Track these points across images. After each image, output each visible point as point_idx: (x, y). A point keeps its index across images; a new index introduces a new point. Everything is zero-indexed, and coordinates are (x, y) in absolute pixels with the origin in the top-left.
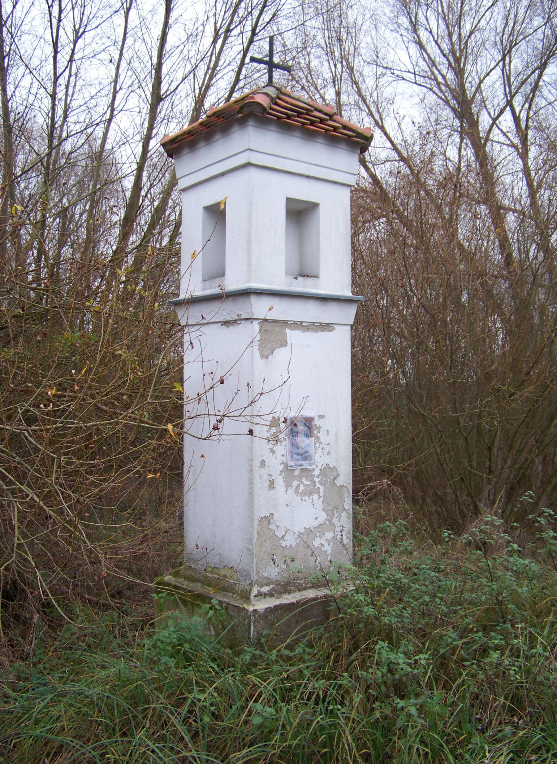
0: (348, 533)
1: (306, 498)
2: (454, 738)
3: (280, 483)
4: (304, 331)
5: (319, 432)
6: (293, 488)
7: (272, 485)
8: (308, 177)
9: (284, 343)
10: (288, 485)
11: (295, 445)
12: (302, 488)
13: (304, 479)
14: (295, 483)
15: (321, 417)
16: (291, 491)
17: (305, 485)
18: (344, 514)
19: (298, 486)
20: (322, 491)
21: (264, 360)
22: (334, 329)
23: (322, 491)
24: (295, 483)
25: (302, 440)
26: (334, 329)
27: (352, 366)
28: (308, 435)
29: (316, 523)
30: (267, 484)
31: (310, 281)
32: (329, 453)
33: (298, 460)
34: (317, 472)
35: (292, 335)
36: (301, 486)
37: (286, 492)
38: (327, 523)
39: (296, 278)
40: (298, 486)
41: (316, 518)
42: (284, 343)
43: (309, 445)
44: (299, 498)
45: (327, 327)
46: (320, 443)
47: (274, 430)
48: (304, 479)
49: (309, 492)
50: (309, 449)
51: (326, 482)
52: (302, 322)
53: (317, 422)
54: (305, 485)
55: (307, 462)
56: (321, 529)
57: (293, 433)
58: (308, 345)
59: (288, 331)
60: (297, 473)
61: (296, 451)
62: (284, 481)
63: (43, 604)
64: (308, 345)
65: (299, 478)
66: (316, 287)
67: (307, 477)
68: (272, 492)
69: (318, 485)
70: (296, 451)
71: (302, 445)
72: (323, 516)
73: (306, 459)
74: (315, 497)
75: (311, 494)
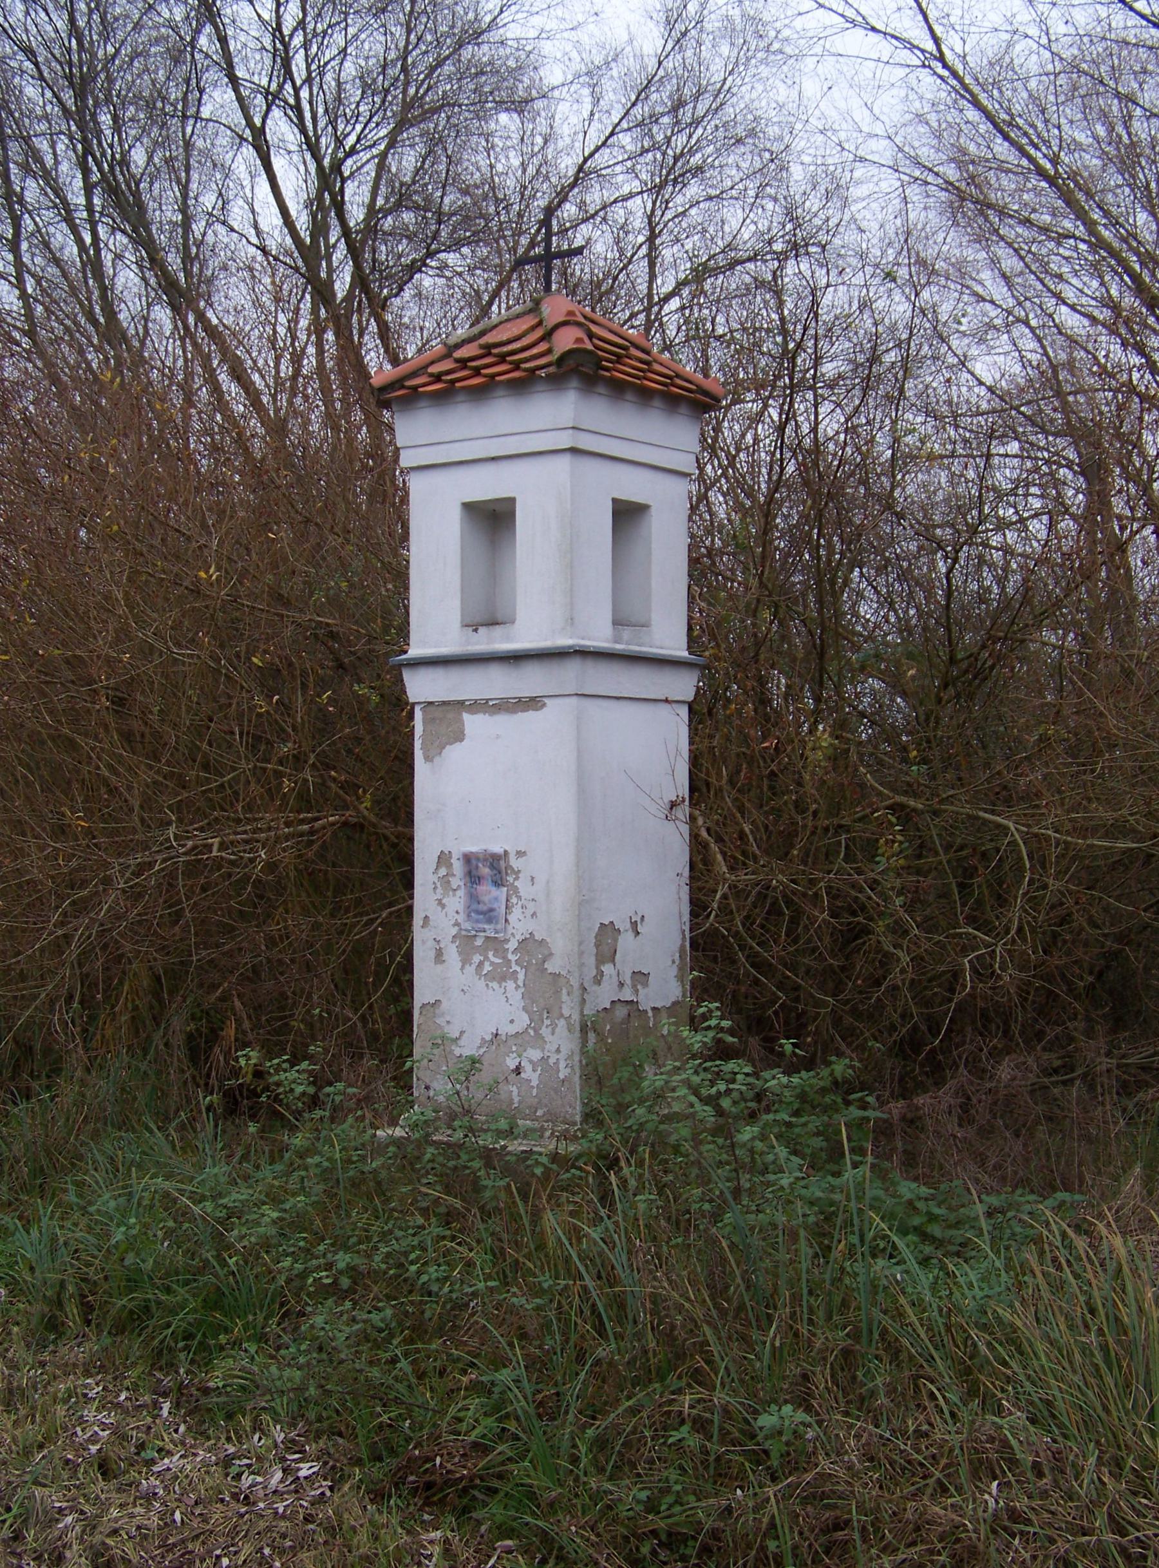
0: (569, 1057)
1: (495, 985)
2: (827, 1553)
3: (452, 954)
4: (492, 714)
5: (517, 879)
6: (474, 966)
7: (439, 956)
8: (493, 459)
9: (459, 737)
10: (466, 961)
11: (473, 898)
12: (487, 967)
13: (490, 954)
14: (477, 958)
15: (520, 854)
16: (470, 969)
17: (492, 963)
18: (562, 1023)
19: (481, 964)
20: (521, 976)
21: (429, 765)
22: (544, 705)
23: (521, 976)
24: (477, 958)
25: (490, 893)
26: (544, 705)
27: (412, 783)
28: (498, 883)
29: (512, 1029)
30: (432, 954)
31: (498, 631)
32: (534, 915)
33: (477, 921)
34: (512, 945)
35: (472, 722)
36: (487, 964)
37: (462, 968)
38: (532, 1032)
39: (476, 630)
40: (481, 964)
41: (512, 1021)
42: (459, 737)
43: (496, 899)
44: (482, 982)
45: (533, 703)
46: (520, 898)
47: (443, 871)
48: (490, 954)
49: (501, 976)
50: (495, 906)
51: (529, 962)
52: (487, 700)
53: (514, 863)
54: (492, 963)
55: (492, 926)
56: (530, 1037)
57: (473, 878)
58: (498, 737)
59: (466, 716)
60: (479, 942)
61: (475, 906)
62: (460, 953)
63: (382, 1061)
64: (498, 737)
65: (483, 950)
66: (508, 639)
67: (496, 951)
68: (439, 967)
69: (515, 967)
70: (475, 906)
71: (486, 899)
72: (523, 1020)
73: (490, 921)
74: (510, 985)
75: (503, 979)
